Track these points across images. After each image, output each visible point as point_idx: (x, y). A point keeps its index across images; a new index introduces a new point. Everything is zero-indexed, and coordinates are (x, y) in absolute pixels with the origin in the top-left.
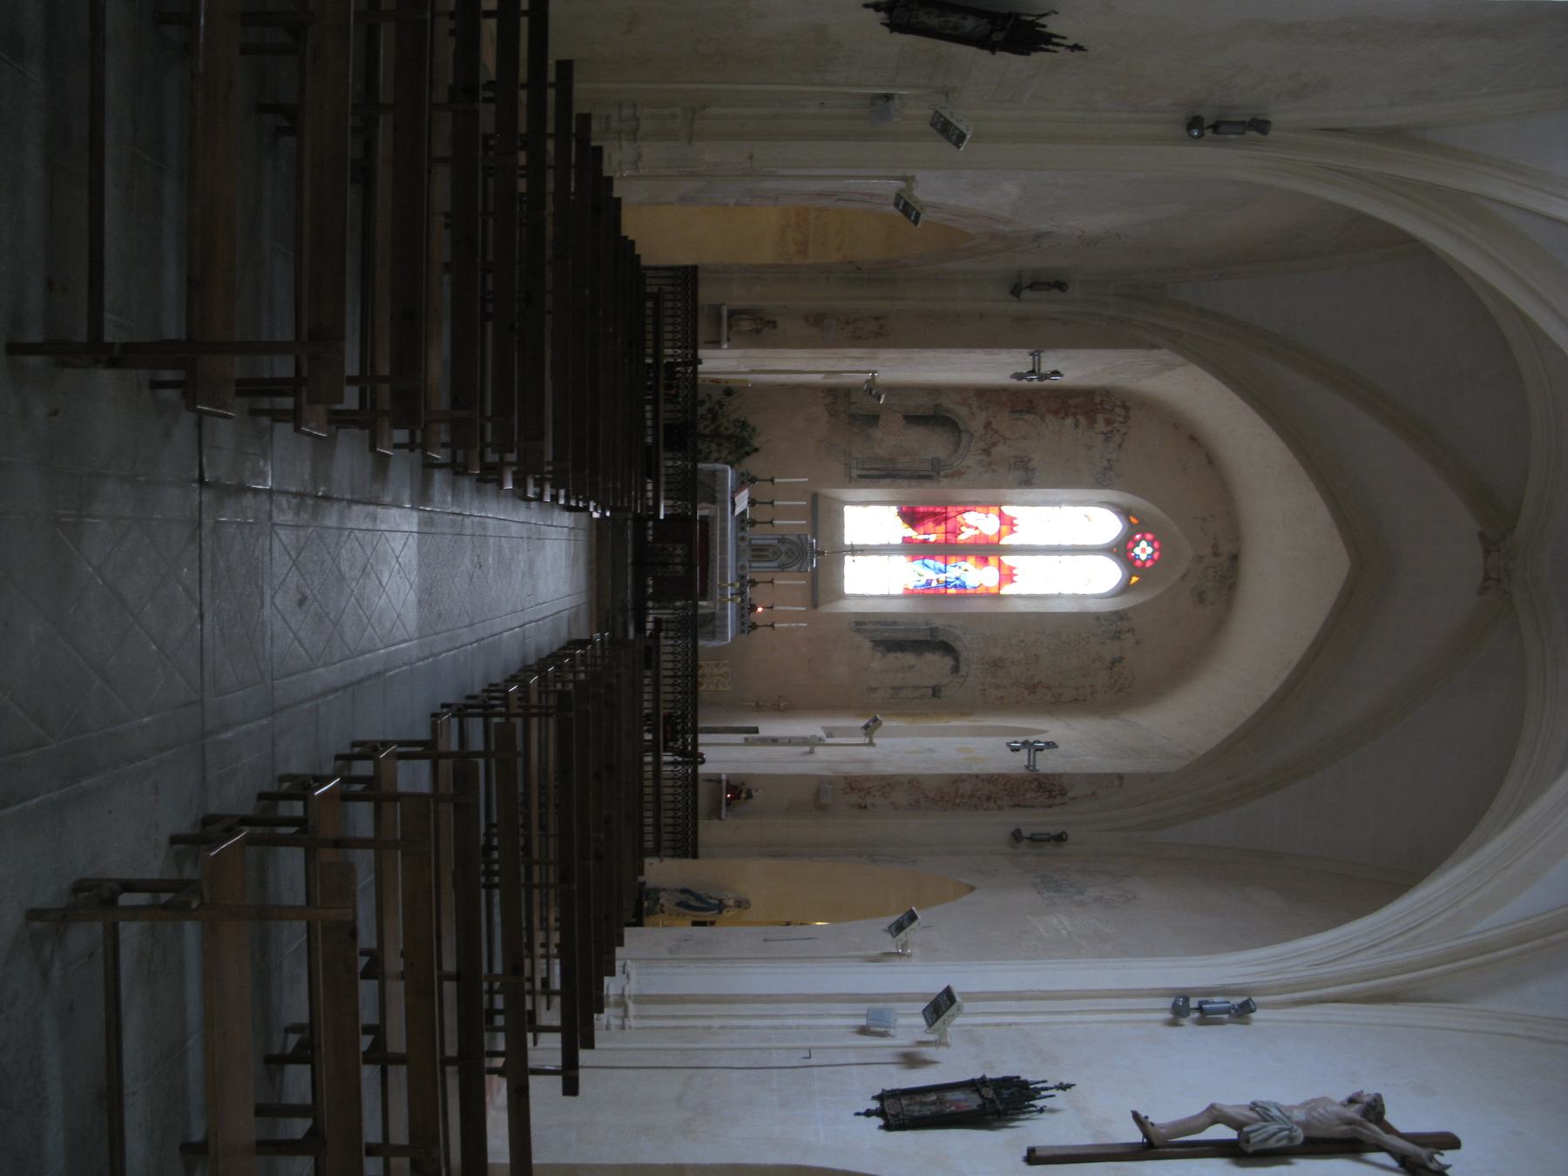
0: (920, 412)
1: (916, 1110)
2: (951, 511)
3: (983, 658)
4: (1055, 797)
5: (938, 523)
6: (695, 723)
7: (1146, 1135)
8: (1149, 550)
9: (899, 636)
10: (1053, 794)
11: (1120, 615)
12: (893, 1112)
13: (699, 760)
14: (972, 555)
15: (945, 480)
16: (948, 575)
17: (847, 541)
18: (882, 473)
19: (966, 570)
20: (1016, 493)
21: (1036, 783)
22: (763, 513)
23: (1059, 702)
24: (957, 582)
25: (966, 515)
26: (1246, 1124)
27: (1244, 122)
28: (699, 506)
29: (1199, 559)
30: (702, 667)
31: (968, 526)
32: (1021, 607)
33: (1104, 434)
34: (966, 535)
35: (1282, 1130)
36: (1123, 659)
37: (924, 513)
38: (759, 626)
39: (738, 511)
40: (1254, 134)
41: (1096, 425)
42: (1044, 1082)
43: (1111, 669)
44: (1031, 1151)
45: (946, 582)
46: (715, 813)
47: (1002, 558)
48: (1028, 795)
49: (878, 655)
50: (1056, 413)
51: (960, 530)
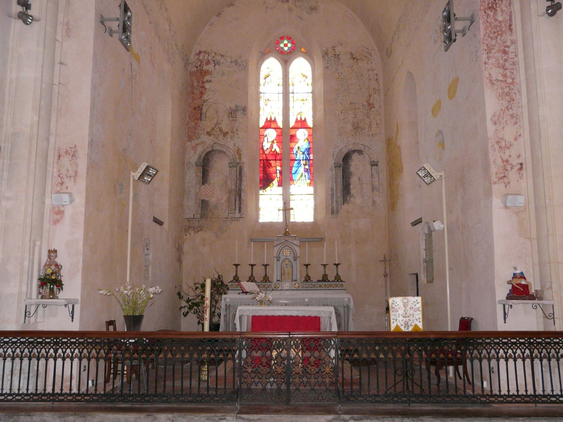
5: (270, 165)
9: (340, 187)
11: (325, 54)
21: (489, 12)
22: (259, 272)
25: (265, 148)
31: (272, 147)
32: (320, 114)
41: (210, 70)
49: (352, 199)
51: (274, 151)
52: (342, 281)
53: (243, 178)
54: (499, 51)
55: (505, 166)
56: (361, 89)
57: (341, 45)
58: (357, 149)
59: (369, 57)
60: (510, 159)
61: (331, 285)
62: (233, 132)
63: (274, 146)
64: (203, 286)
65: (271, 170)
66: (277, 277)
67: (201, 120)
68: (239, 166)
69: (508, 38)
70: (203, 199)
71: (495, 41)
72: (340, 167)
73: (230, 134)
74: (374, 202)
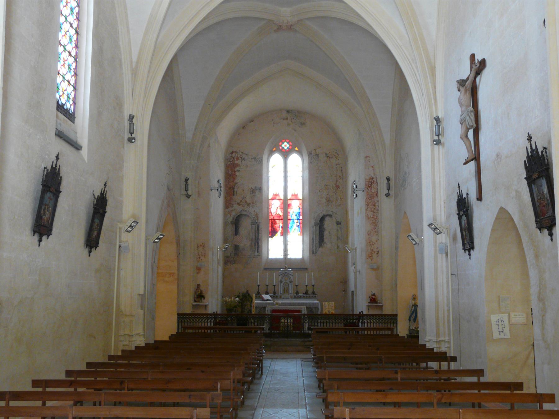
0: (234, 229)
1: (468, 238)
2: (271, 218)
3: (326, 206)
4: (374, 181)
5: (275, 223)
6: (350, 315)
7: (472, 160)
8: (285, 143)
9: (318, 237)
10: (372, 182)
11: (310, 154)
12: (468, 246)
13: (361, 313)
14: (287, 210)
15: (259, 220)
16: (295, 219)
17: (282, 257)
18: (256, 243)
19: (293, 212)
20: (264, 193)
21: (369, 188)
22: (271, 289)
23: (342, 177)
24: (298, 215)
25: (272, 212)
26: (467, 127)
27: (130, 124)
28: (267, 313)
29: (288, 125)
30: (326, 312)
31: (277, 211)
32: (307, 191)
33: (242, 160)
34: (280, 213)
35: (468, 115)
36: (326, 153)
37: (271, 228)
38: (313, 290)
39: (270, 298)
40: (134, 120)
41: (239, 164)
42: (458, 193)
43: (330, 157)
44: (478, 199)
45: (298, 220)
46: (381, 307)
47: (288, 198)
48: (373, 191)
49: (325, 245)
50: (234, 179)
51: (278, 214)
52: (316, 294)
53: (259, 232)
54: (372, 205)
55: (372, 252)
56: (331, 176)
57: (320, 148)
58: (328, 214)
59: (337, 155)
60: (374, 249)
61: (309, 297)
62: (253, 203)
63: (278, 211)
64: (380, 303)
65: (276, 226)
66: (281, 292)
67: (234, 195)
68: (257, 224)
69: (376, 199)
70: (235, 244)
71: (370, 201)
72: (318, 225)
73: (251, 204)
74: (338, 247)
